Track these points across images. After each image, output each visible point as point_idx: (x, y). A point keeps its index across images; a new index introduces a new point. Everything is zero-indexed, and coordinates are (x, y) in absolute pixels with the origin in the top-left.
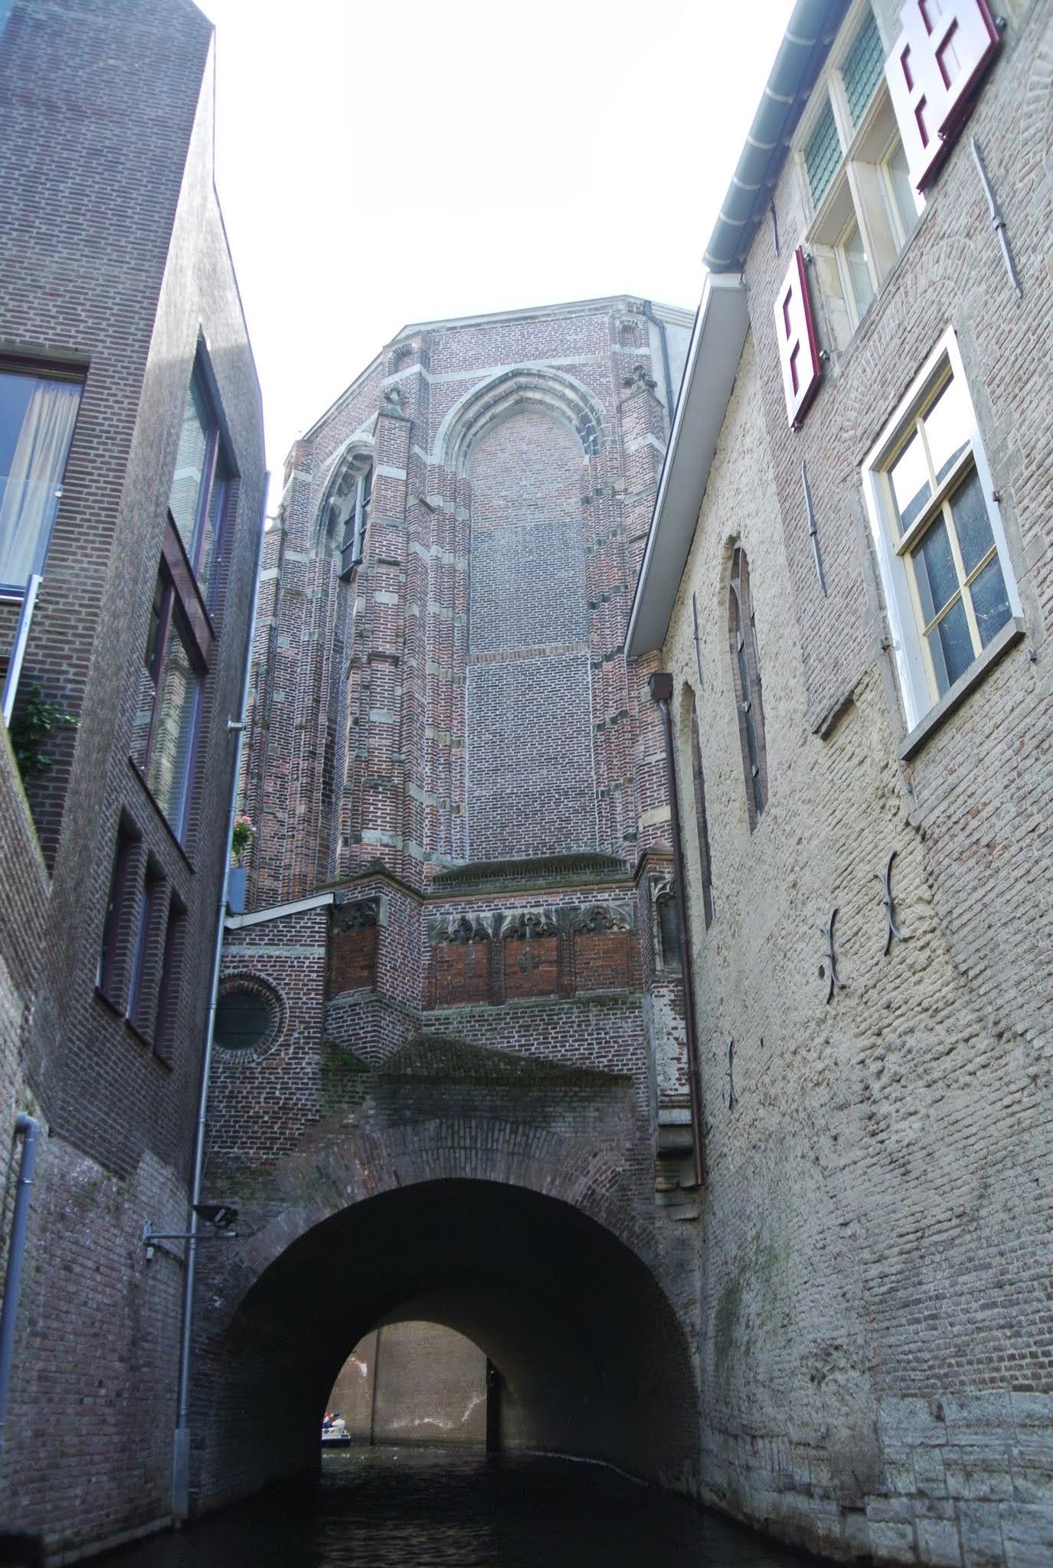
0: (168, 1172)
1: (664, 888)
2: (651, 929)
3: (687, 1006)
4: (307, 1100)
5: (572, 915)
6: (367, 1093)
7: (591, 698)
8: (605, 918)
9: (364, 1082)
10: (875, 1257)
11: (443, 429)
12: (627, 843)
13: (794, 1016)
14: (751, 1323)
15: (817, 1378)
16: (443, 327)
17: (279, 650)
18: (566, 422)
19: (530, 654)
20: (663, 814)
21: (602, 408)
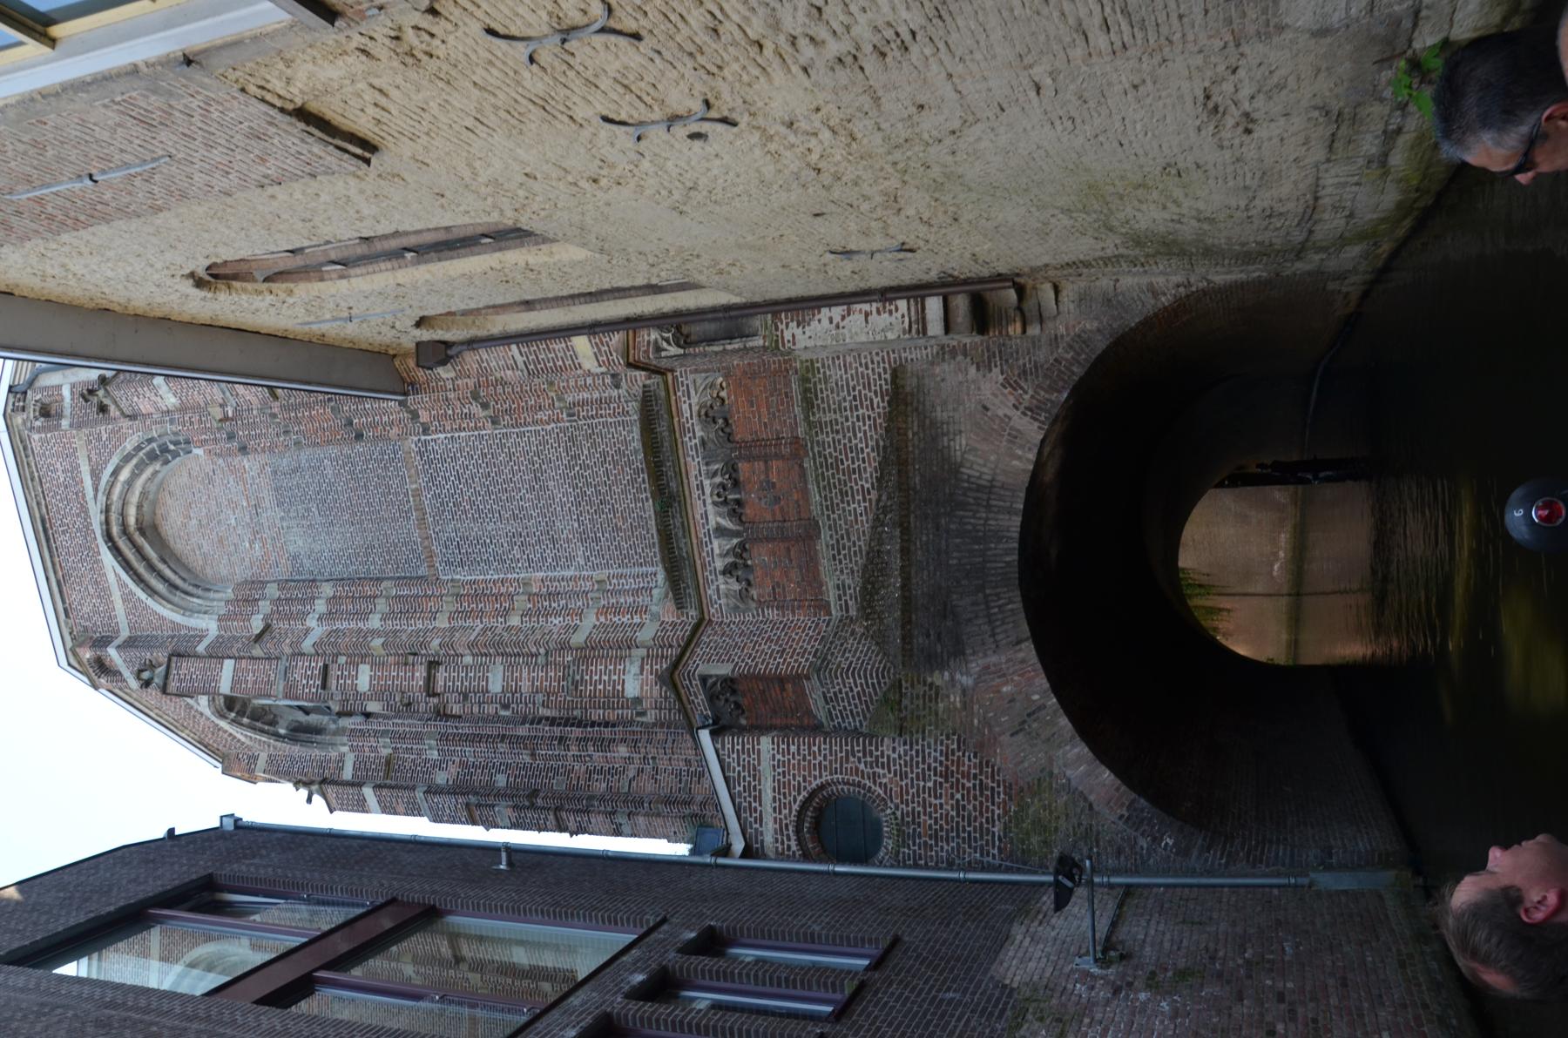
0: (1018, 931)
1: (667, 340)
2: (716, 353)
3: (804, 306)
4: (935, 751)
5: (710, 445)
6: (925, 682)
7: (463, 434)
8: (711, 407)
9: (912, 686)
10: (1080, 40)
11: (177, 617)
12: (623, 383)
13: (769, 170)
14: (1175, 217)
15: (1248, 124)
16: (66, 624)
17: (451, 783)
18: (160, 476)
19: (420, 508)
20: (582, 344)
21: (135, 438)
